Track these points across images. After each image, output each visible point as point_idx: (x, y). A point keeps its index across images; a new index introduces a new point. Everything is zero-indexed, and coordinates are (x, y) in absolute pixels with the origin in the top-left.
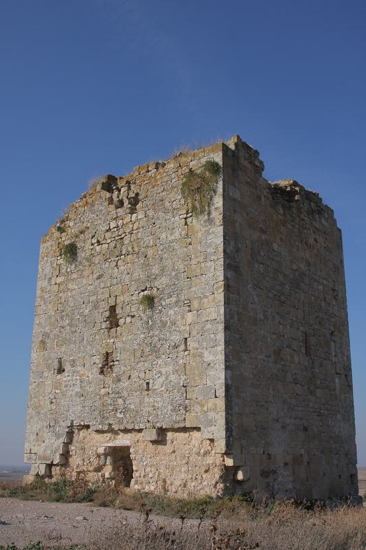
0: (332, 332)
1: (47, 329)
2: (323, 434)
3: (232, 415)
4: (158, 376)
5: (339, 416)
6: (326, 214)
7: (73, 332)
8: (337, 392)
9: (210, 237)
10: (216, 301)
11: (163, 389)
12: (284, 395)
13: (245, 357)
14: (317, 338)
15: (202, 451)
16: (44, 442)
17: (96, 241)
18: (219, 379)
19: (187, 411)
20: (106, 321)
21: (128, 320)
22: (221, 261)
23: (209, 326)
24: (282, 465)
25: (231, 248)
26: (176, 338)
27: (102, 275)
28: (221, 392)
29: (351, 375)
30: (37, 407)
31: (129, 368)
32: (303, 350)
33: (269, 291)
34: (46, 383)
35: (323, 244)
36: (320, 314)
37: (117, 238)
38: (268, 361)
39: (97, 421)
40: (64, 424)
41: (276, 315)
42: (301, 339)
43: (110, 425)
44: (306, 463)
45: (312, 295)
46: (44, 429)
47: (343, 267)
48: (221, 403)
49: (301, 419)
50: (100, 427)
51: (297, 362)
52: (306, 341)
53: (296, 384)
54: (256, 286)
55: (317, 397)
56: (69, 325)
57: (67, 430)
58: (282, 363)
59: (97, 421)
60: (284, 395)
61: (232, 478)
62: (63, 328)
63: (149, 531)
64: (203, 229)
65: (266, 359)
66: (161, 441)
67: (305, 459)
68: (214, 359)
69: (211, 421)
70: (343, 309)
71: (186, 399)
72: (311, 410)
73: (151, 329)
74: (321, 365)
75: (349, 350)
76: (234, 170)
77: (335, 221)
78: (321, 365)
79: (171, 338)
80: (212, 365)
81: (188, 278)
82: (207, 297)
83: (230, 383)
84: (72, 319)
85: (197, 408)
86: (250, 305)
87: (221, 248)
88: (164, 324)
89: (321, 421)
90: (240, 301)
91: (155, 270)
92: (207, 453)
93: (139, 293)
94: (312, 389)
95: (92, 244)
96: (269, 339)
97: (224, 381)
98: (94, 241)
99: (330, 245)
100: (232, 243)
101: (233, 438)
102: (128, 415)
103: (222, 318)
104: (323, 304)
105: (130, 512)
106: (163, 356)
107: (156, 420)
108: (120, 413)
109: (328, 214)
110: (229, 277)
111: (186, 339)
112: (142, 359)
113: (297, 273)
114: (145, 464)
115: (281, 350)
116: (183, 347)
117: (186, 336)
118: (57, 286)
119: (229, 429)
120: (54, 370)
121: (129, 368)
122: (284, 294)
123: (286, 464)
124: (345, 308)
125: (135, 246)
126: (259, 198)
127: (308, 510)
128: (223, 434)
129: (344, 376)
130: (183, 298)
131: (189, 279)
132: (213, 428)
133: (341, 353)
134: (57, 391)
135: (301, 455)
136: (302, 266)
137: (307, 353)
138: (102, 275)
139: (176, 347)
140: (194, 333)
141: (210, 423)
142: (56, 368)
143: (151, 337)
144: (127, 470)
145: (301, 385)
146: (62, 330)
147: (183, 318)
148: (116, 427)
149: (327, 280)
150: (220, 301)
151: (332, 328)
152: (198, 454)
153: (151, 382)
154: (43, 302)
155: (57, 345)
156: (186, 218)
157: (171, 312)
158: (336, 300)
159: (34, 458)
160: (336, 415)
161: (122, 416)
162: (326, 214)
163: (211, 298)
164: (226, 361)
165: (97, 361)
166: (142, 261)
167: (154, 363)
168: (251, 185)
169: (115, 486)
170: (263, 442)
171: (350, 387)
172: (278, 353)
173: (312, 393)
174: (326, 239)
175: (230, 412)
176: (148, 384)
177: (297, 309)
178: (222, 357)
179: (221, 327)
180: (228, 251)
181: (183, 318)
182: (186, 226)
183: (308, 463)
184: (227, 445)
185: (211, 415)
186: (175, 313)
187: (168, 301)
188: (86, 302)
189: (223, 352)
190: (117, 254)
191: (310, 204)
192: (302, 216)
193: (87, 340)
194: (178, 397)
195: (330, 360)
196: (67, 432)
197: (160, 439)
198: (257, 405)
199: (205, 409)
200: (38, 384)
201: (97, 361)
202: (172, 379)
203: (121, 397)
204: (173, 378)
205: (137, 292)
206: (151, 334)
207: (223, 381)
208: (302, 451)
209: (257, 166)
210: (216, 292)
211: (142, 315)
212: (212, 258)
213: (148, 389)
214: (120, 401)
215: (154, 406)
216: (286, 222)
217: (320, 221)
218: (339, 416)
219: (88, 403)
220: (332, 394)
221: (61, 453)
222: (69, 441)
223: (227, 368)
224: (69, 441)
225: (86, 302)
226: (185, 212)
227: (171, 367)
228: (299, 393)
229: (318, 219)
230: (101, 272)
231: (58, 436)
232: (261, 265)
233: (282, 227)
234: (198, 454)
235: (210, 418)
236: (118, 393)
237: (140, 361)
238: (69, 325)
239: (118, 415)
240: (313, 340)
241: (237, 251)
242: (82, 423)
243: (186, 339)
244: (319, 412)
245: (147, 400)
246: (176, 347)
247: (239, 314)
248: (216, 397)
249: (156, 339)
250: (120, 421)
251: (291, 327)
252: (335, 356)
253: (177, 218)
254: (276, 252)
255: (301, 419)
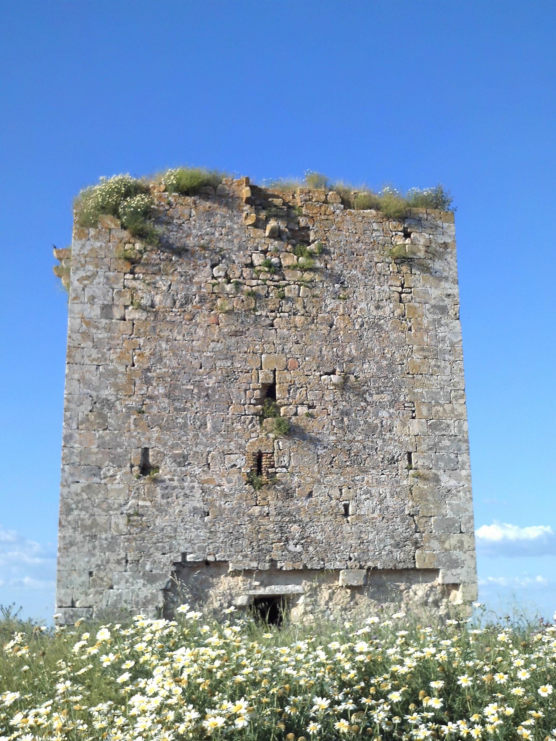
4: (364, 497)
20: (255, 405)
31: (309, 479)
56: (168, 396)
59: (245, 556)
63: (25, 713)
68: (457, 485)
85: (435, 544)
93: (321, 376)
105: (231, 455)
108: (296, 545)
111: (409, 454)
117: (411, 449)
120: (132, 466)
126: (395, 228)
132: (459, 570)
133: (40, 639)
143: (350, 442)
144: (30, 703)
156: (401, 293)
157: (384, 414)
163: (448, 407)
165: (240, 463)
167: (357, 478)
169: (29, 693)
182: (401, 304)
186: (391, 416)
194: (204, 683)
198: (465, 553)
199: (447, 545)
203: (295, 522)
204: (390, 501)
229: (464, 621)
237: (331, 473)
239: (291, 547)
246: (393, 461)
250: (296, 557)
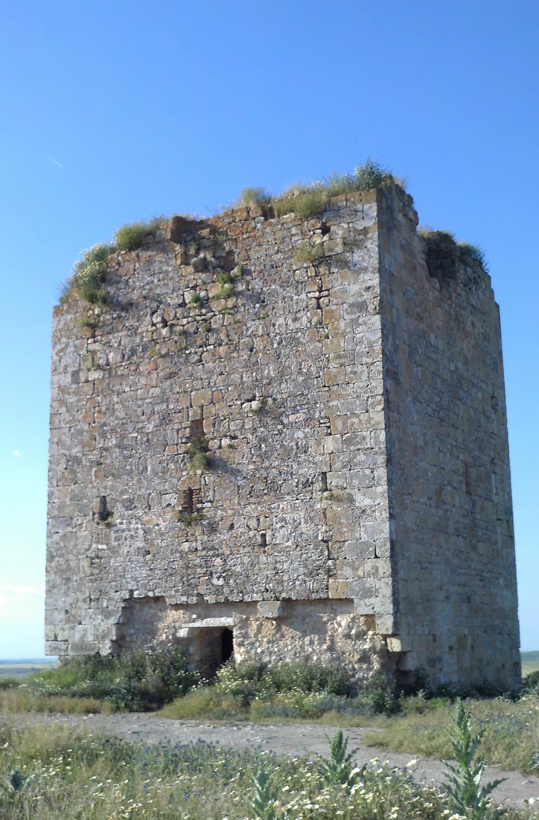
0: (493, 459)
1: (76, 451)
2: (486, 606)
3: (398, 583)
5: (501, 581)
6: (483, 282)
7: (126, 458)
8: (499, 545)
9: (360, 329)
10: (372, 422)
11: (287, 544)
12: (447, 553)
13: (407, 500)
14: (478, 470)
15: (353, 632)
16: (80, 623)
17: (159, 319)
18: (382, 531)
19: (330, 576)
20: (186, 443)
21: (225, 442)
22: (379, 366)
23: (361, 457)
24: (447, 649)
25: (390, 347)
26: (307, 471)
27: (176, 374)
28: (385, 550)
29: (513, 521)
30: (63, 571)
31: (230, 512)
32: (464, 488)
33: (428, 405)
34: (79, 534)
35: (482, 330)
36: (480, 434)
37: (198, 318)
38: (430, 506)
39: (177, 591)
40: (117, 596)
41: (436, 439)
42: (461, 471)
43: (199, 595)
44: (469, 647)
45: (471, 407)
46: (80, 604)
47: (501, 361)
48: (385, 565)
49: (464, 585)
50: (184, 599)
51: (458, 505)
52: (467, 475)
53: (458, 536)
54: (416, 400)
55: (478, 554)
56: (118, 446)
57: (123, 605)
58: (444, 507)
59: (177, 591)
60: (447, 553)
61: (395, 667)
62: (106, 450)
64: (347, 317)
65: (428, 502)
66: (286, 618)
67: (469, 642)
69: (370, 590)
70: (503, 425)
71: (329, 559)
72: (474, 572)
73: (264, 456)
74: (482, 509)
75: (509, 485)
76: (389, 230)
77: (492, 292)
78: (482, 509)
79: (300, 472)
80: (369, 512)
81: (325, 386)
82: (357, 416)
83: (394, 537)
84: (123, 437)
85: (348, 572)
86: (410, 425)
87: (378, 347)
88: (287, 452)
89: (484, 587)
90: (400, 421)
91: (271, 371)
92: (361, 636)
93: (242, 404)
94: (473, 542)
95: (153, 325)
96: (430, 474)
97: (388, 535)
98: (157, 319)
99: (488, 330)
100: (390, 338)
101: (400, 613)
102: (231, 581)
103: (383, 446)
104: (483, 419)
106: (288, 497)
107: (280, 589)
108: (218, 578)
109: (485, 282)
110: (388, 387)
111: (325, 474)
112: (252, 500)
113: (455, 376)
114: (259, 651)
115: (442, 489)
116: (318, 485)
117: (325, 469)
118: (91, 385)
119: (396, 602)
120: (94, 514)
121: (230, 512)
122: (443, 409)
123: (451, 648)
124: (504, 423)
125: (232, 333)
127: (329, 203)
128: (390, 608)
129: (505, 522)
130: (317, 415)
131: (326, 389)
132: (372, 600)
134: (100, 547)
135: (465, 635)
136: (460, 365)
137: (468, 492)
138: (176, 374)
139: (308, 484)
140: (338, 465)
141: (368, 593)
142: (97, 510)
145: (463, 537)
146: (104, 454)
147: (318, 443)
148: (210, 599)
149: (486, 383)
150: (379, 423)
151: (492, 454)
152: (348, 636)
153: (269, 533)
154: (64, 409)
155: (96, 476)
156: (318, 299)
158: (496, 411)
159: (64, 647)
160: (498, 579)
161: (221, 582)
162: (483, 282)
163: (364, 417)
164: (390, 508)
165: (174, 502)
166: (246, 357)
167: (273, 506)
168: (94, 390)
170: (428, 618)
171: (511, 537)
172: (439, 492)
173: (474, 548)
174: (484, 321)
175: (396, 578)
176: (264, 536)
177: (457, 428)
178: (385, 503)
179: (381, 459)
180: (387, 351)
181: (318, 443)
182: (319, 311)
183: (472, 646)
184: (396, 625)
185: (370, 582)
186: (306, 437)
187: (292, 418)
188: (148, 412)
189: (386, 495)
190: (199, 342)
191: (466, 271)
192: (459, 291)
193: (153, 470)
195: (491, 500)
196: (123, 608)
197: (128, 606)
199: (360, 573)
200: (65, 536)
201: (174, 502)
202: (304, 530)
203: (218, 556)
205: (239, 402)
206: (267, 464)
207: (386, 534)
208: (466, 631)
209: (411, 219)
210: (371, 410)
211: (250, 436)
212: (365, 360)
213: (264, 544)
214: (218, 561)
215: (275, 568)
216: (442, 300)
217: (477, 295)
218: (501, 581)
219: (160, 564)
220: (493, 550)
221: (114, 638)
222: (125, 621)
223: (392, 516)
224: (125, 621)
225: (148, 412)
226: (316, 288)
227: (302, 514)
228: (462, 550)
230: (173, 369)
231: (107, 615)
232: (419, 368)
233: (438, 308)
234: (348, 636)
235: (368, 585)
236: (213, 548)
237: (250, 504)
238: (118, 446)
239: (215, 581)
240: (473, 472)
241: (395, 351)
242: (151, 594)
243: (325, 474)
244: (482, 576)
245: (263, 558)
247: (400, 440)
248: (376, 557)
249: (275, 472)
250: (218, 590)
251: (451, 455)
252: (496, 494)
253: (303, 296)
254: (434, 346)
255: (464, 585)
